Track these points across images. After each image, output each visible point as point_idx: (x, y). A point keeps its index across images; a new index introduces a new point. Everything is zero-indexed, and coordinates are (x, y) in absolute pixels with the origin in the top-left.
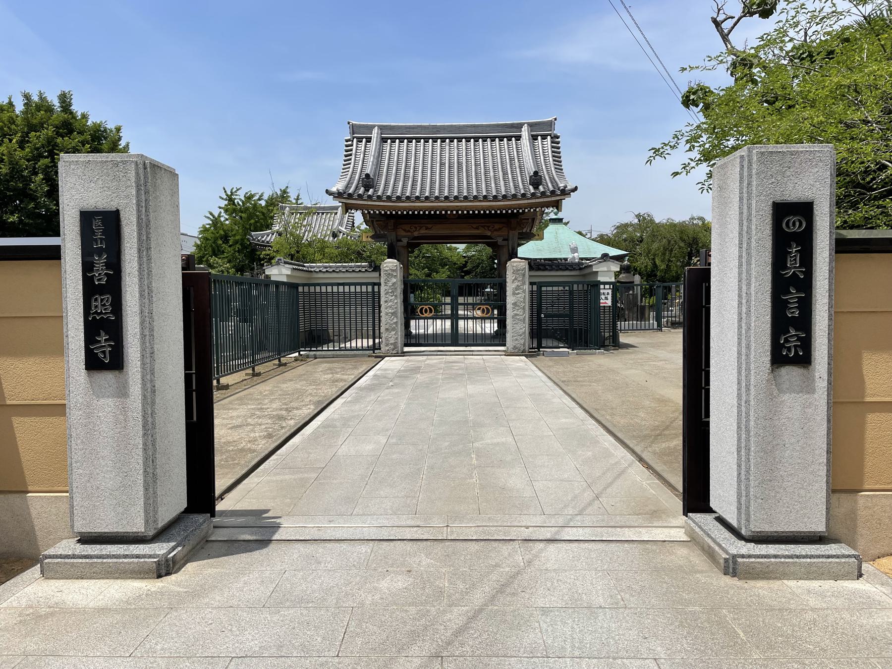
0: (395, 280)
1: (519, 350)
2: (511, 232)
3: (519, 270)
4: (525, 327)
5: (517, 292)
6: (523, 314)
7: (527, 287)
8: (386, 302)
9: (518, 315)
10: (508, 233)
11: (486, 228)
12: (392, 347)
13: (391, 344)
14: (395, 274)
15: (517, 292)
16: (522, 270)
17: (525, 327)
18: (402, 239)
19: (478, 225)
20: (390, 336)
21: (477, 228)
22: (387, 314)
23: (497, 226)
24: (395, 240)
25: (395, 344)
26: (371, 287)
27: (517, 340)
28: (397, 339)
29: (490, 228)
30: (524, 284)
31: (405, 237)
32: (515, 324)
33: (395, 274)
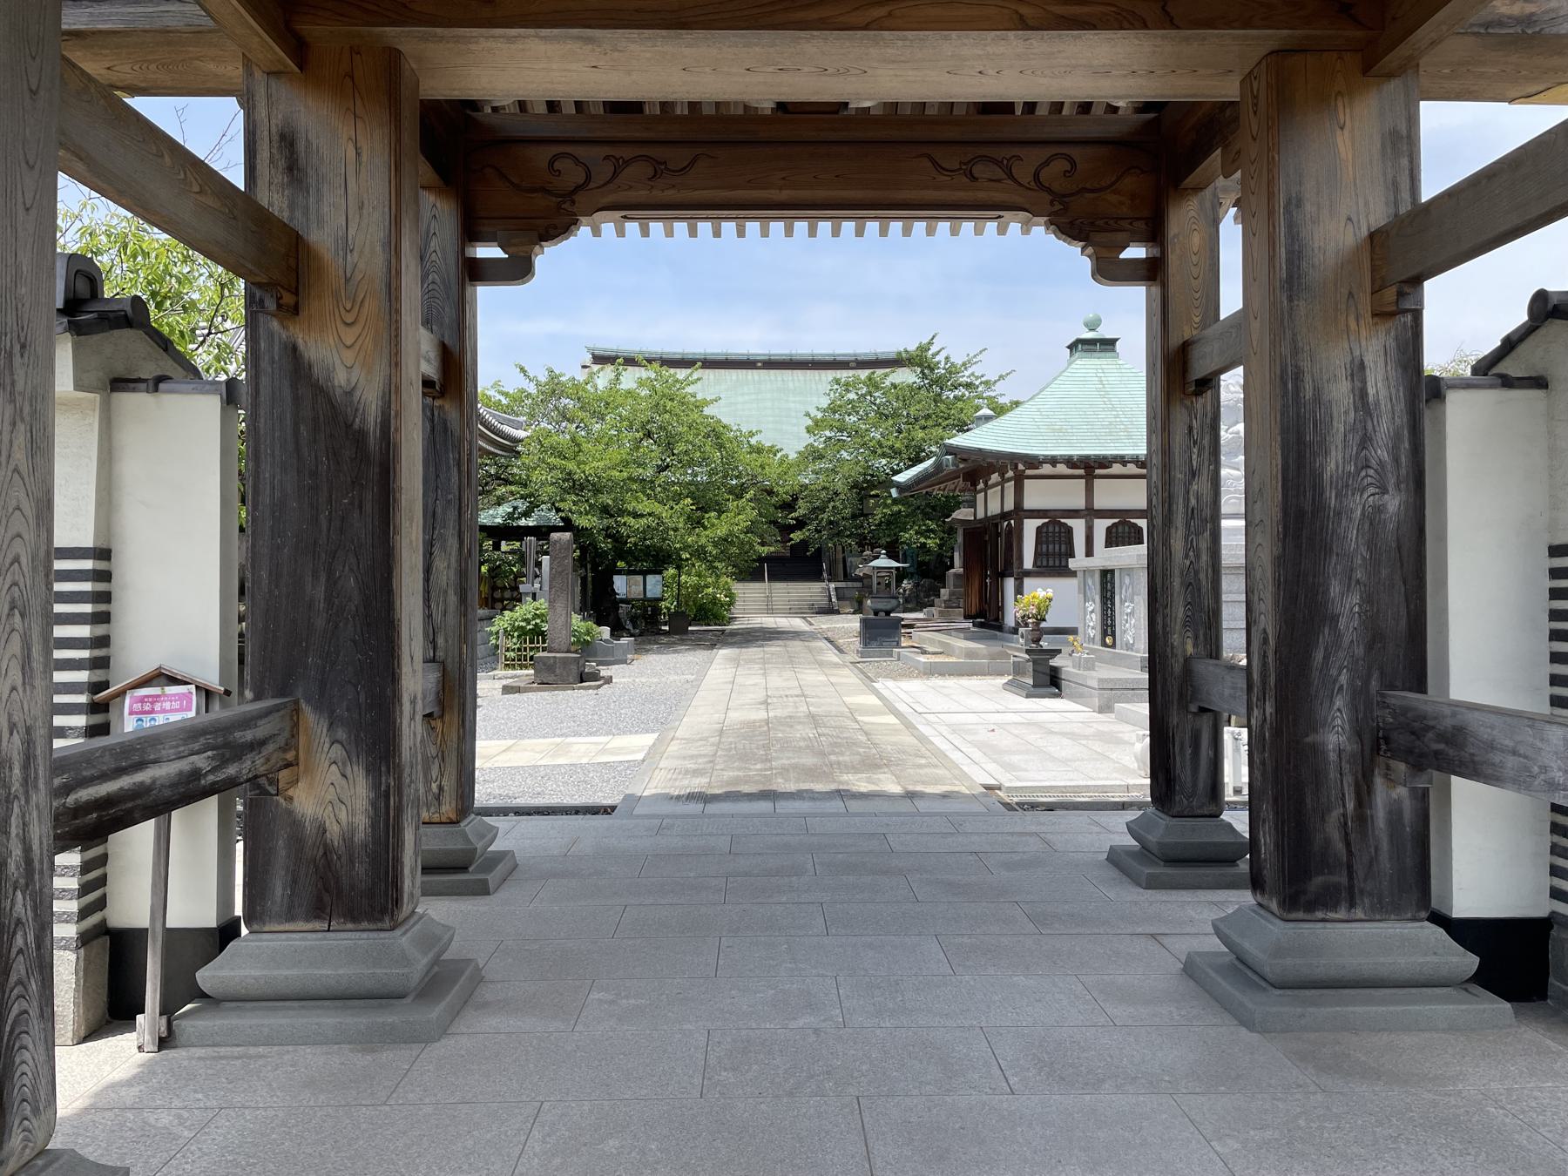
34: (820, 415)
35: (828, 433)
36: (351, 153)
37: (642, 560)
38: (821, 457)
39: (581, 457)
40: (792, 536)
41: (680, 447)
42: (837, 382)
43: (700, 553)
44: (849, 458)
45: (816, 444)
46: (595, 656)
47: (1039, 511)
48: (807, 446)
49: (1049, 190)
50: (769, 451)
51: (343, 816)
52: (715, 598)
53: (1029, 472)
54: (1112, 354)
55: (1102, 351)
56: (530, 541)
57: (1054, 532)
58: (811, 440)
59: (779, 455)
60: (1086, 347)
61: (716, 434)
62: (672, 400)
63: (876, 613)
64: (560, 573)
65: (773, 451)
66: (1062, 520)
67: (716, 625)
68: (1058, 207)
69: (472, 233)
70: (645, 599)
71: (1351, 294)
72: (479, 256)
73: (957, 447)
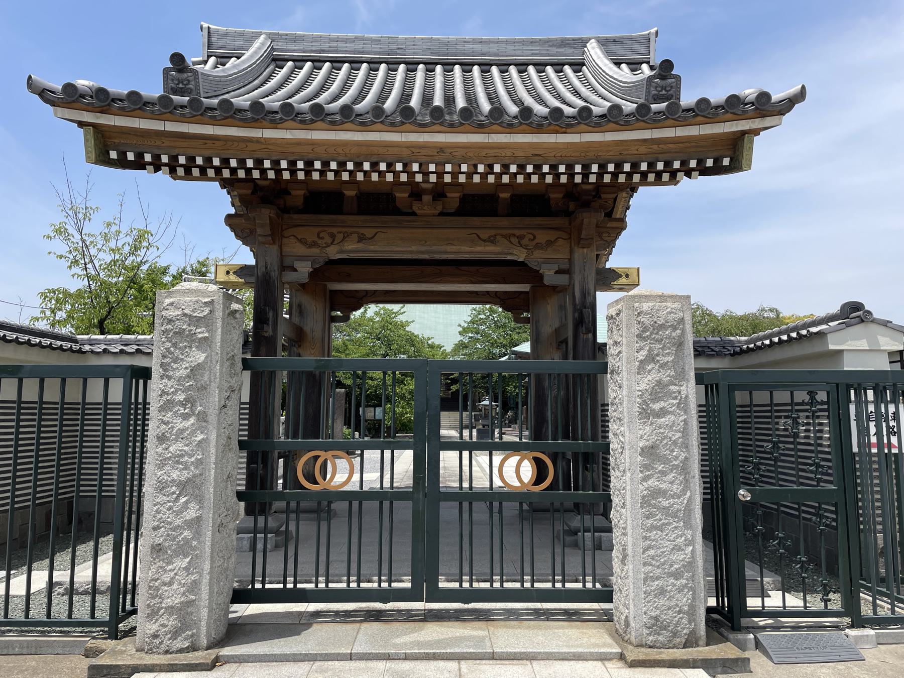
0: (201, 357)
1: (675, 634)
2: (579, 253)
3: (662, 327)
4: (691, 542)
5: (657, 406)
6: (684, 492)
7: (691, 391)
8: (162, 439)
9: (662, 493)
10: (571, 252)
11: (515, 240)
12: (172, 622)
13: (171, 610)
14: (201, 333)
15: (657, 406)
16: (675, 328)
17: (691, 542)
18: (297, 265)
19: (493, 232)
20: (166, 578)
21: (492, 240)
22: (161, 487)
23: (542, 237)
24: (276, 265)
25: (184, 612)
26: (120, 381)
27: (662, 592)
28: (194, 587)
29: (525, 242)
30: (681, 376)
31: (302, 258)
32: (653, 528)
33: (201, 333)
34: (466, 325)
35: (470, 335)
36: (315, 309)
37: (374, 400)
38: (467, 347)
39: (347, 352)
40: (451, 387)
41: (394, 347)
42: (475, 310)
43: (403, 397)
44: (480, 347)
45: (464, 340)
48: (459, 342)
49: (499, 298)
50: (437, 347)
51: (307, 468)
58: (462, 338)
59: (442, 349)
61: (412, 340)
62: (391, 324)
63: (484, 427)
64: (340, 407)
65: (440, 347)
68: (502, 303)
69: (333, 309)
70: (375, 420)
71: (551, 344)
72: (333, 315)
73: (517, 351)
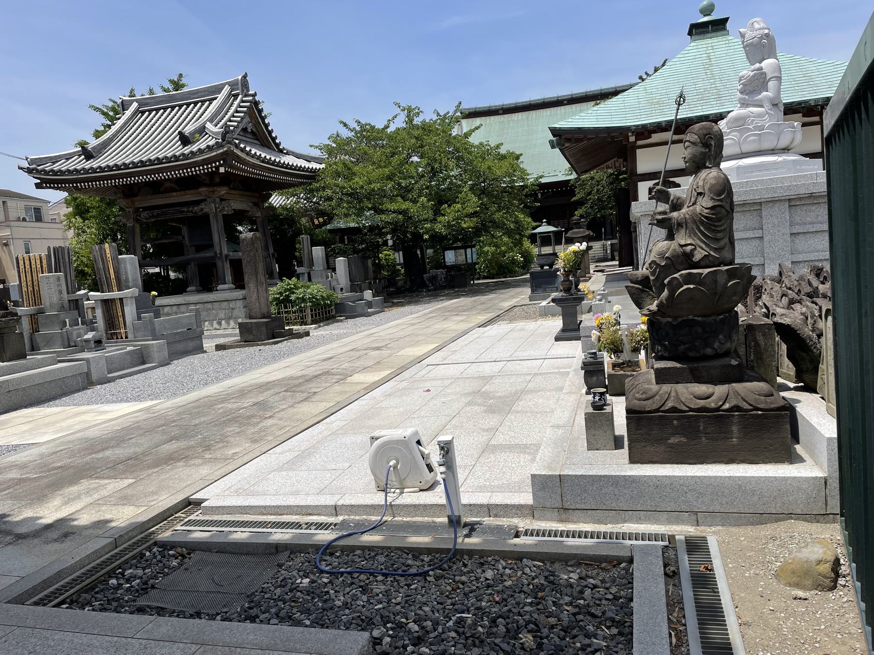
46: (345, 313)
47: (650, 174)
52: (513, 259)
53: (640, 143)
54: (724, 32)
55: (714, 31)
56: (302, 238)
57: (348, 202)
60: (700, 30)
63: (542, 267)
66: (671, 179)
67: (510, 277)
